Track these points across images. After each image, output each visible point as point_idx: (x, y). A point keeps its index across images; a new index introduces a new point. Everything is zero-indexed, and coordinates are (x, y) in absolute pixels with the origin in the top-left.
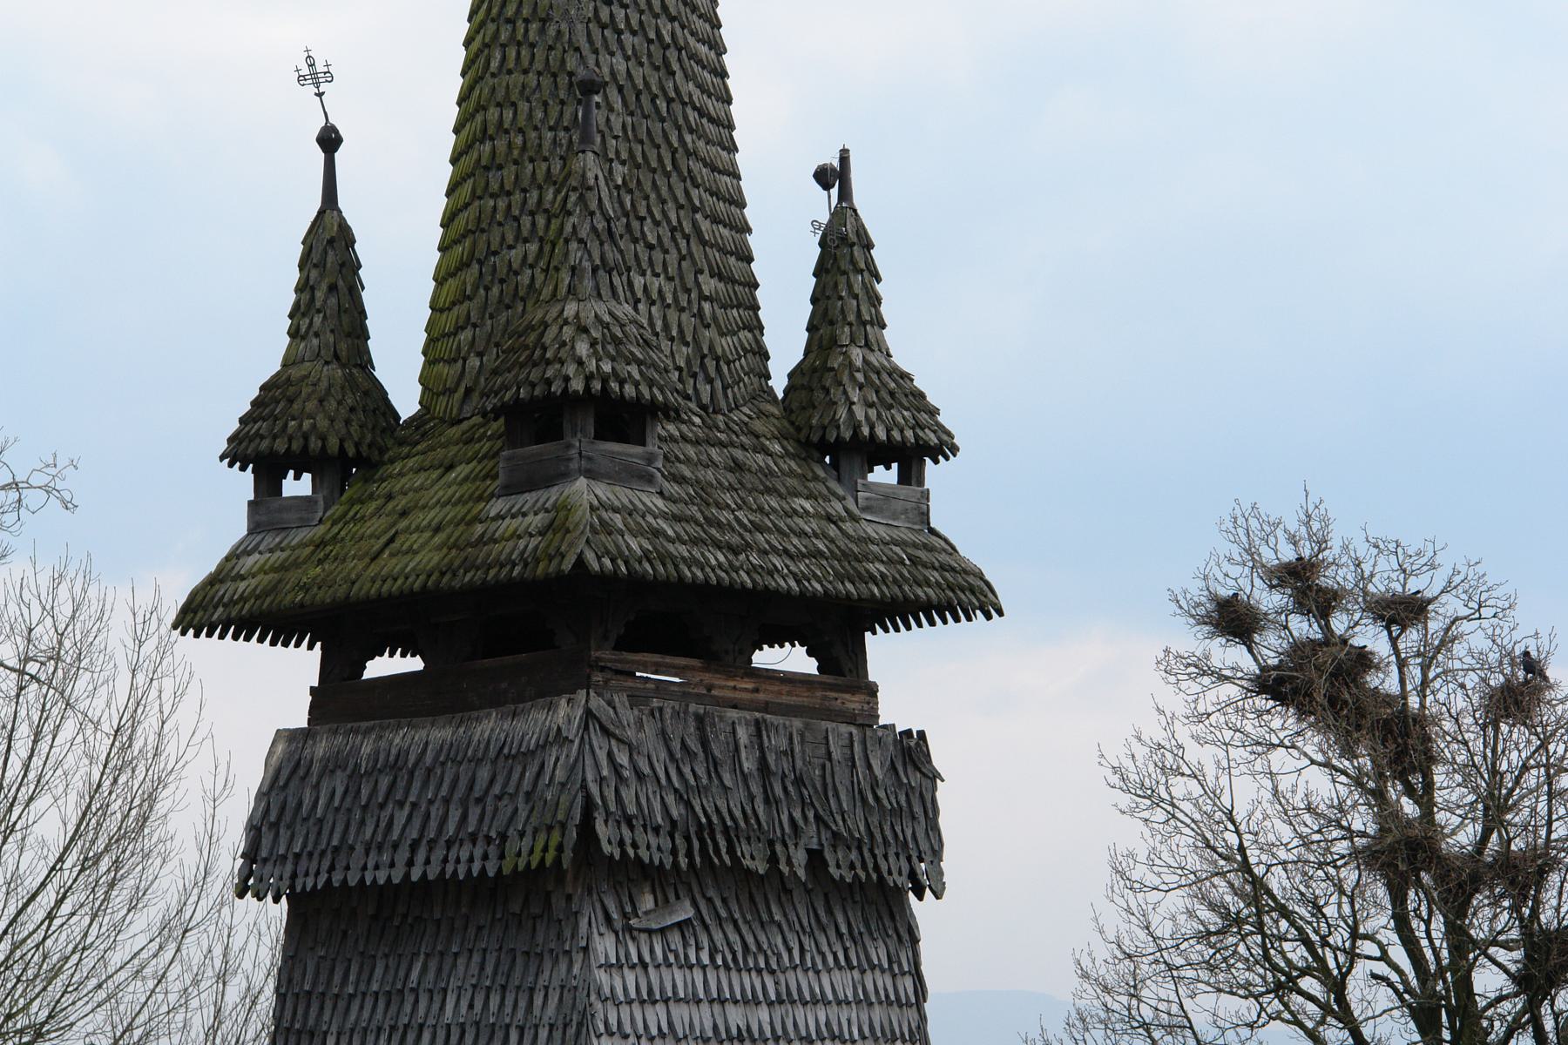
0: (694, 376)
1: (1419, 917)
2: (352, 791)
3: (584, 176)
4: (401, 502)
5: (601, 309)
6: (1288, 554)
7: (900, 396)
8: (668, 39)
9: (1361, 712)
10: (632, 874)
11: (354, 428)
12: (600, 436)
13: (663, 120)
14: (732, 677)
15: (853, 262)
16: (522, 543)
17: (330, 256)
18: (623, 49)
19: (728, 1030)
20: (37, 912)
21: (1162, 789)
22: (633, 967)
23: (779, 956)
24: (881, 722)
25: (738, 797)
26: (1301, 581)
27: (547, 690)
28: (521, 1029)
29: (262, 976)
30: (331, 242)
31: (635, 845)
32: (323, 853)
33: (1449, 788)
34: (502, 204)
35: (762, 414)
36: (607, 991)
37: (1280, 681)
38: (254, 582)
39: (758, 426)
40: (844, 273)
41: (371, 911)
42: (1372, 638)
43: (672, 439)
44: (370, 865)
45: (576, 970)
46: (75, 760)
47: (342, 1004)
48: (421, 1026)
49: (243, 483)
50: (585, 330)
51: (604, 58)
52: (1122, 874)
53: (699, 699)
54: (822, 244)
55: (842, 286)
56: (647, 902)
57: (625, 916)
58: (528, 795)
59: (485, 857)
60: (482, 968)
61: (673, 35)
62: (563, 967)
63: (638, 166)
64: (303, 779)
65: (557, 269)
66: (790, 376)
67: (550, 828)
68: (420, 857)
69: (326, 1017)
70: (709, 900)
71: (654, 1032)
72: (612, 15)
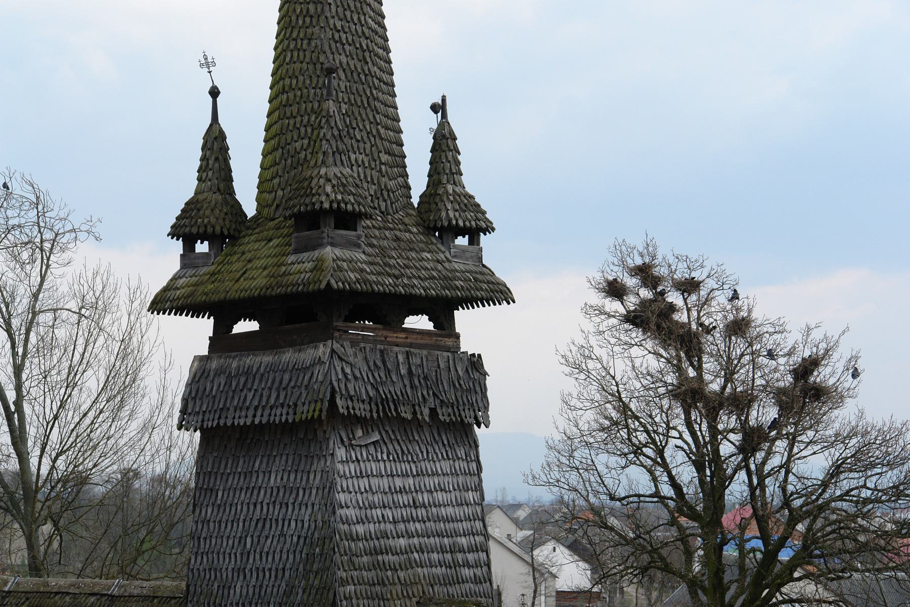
0: (378, 198)
1: (696, 423)
2: (228, 383)
3: (328, 111)
4: (248, 256)
5: (336, 170)
6: (639, 261)
7: (469, 206)
8: (365, 47)
9: (671, 332)
10: (352, 421)
11: (227, 222)
12: (337, 227)
13: (363, 84)
14: (396, 332)
15: (448, 146)
16: (302, 276)
17: (215, 146)
18: (345, 52)
19: (395, 488)
20: (87, 421)
21: (584, 365)
22: (353, 462)
23: (417, 455)
24: (462, 350)
25: (399, 386)
26: (645, 273)
27: (314, 340)
28: (304, 489)
29: (186, 447)
30: (216, 138)
31: (354, 409)
32: (216, 411)
33: (709, 364)
34: (292, 122)
35: (408, 215)
36: (342, 473)
37: (636, 317)
38: (183, 291)
39: (406, 220)
40: (444, 151)
41: (237, 436)
42: (674, 298)
43: (368, 227)
44: (237, 416)
45: (328, 464)
46: (104, 354)
47: (225, 477)
48: (260, 488)
49: (178, 246)
50: (330, 180)
51: (337, 56)
52: (566, 403)
53: (381, 342)
54: (434, 138)
55: (443, 157)
56: (359, 433)
57: (349, 439)
58: (306, 386)
59: (288, 414)
60: (287, 462)
61: (367, 45)
62: (322, 462)
63: (352, 105)
64: (206, 378)
65: (317, 153)
66: (420, 197)
67: (316, 401)
68: (259, 413)
69: (218, 483)
70: (387, 431)
71: (363, 490)
72: (340, 37)
